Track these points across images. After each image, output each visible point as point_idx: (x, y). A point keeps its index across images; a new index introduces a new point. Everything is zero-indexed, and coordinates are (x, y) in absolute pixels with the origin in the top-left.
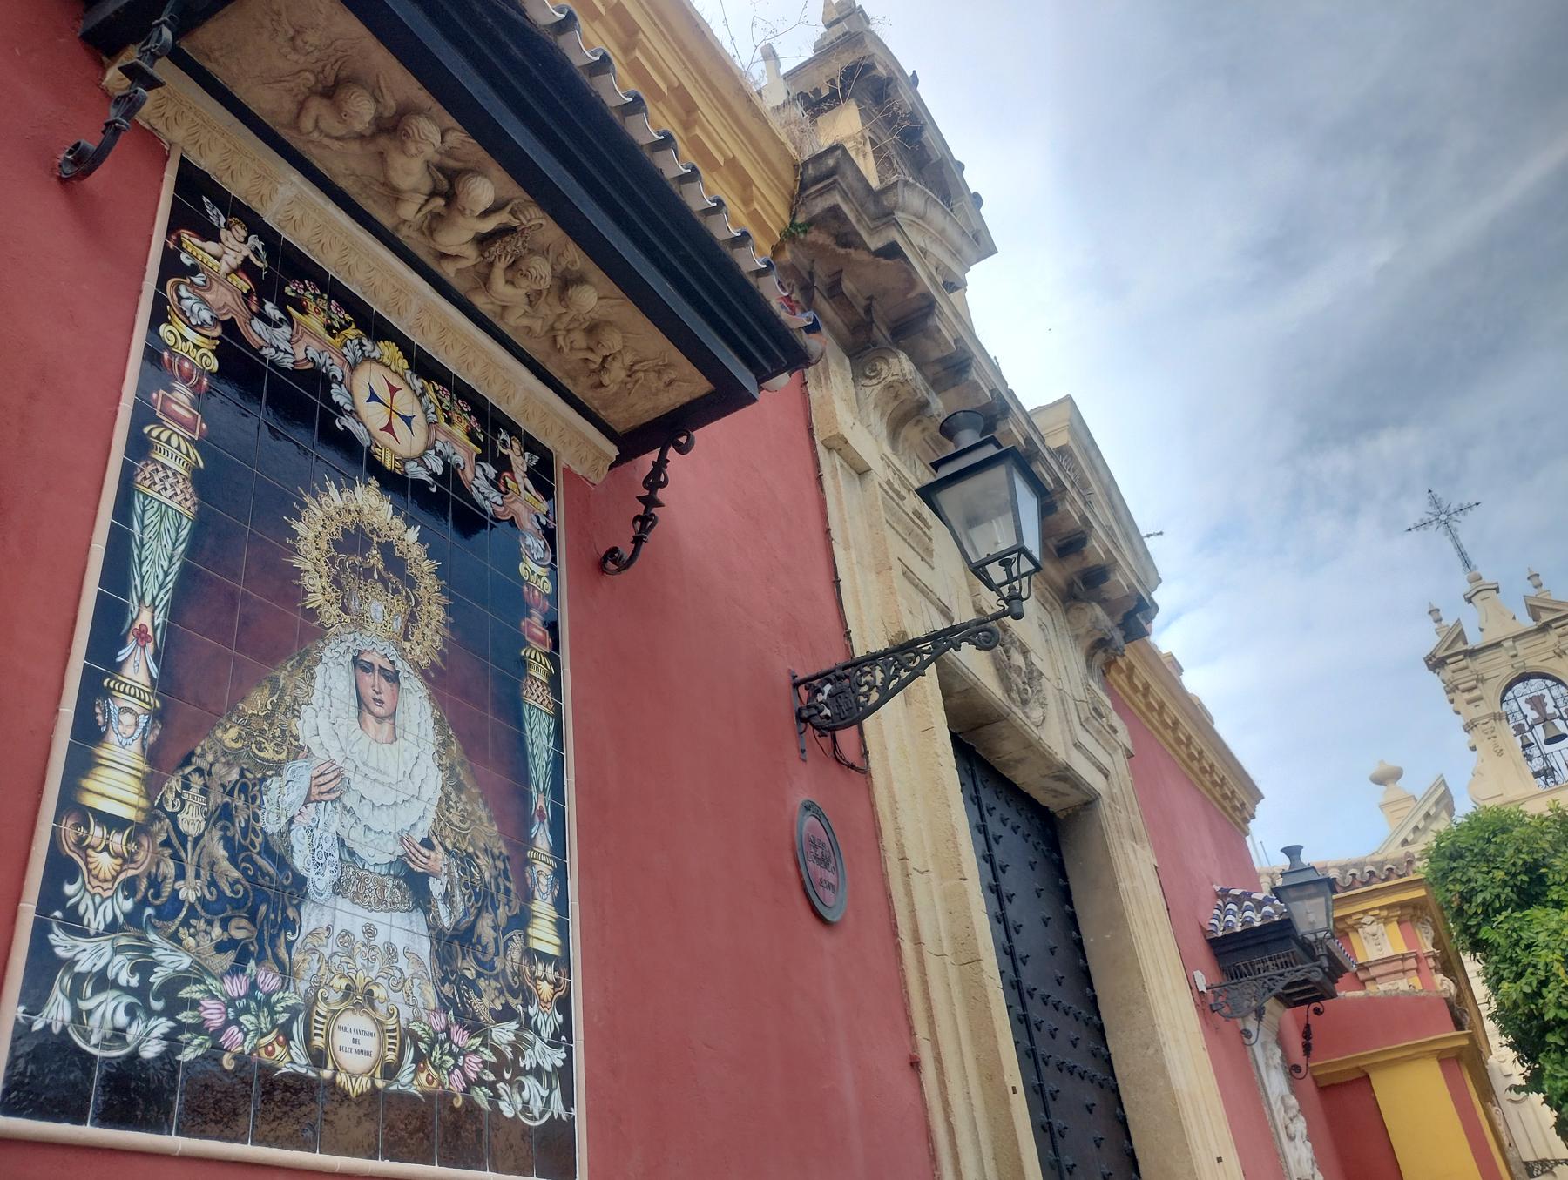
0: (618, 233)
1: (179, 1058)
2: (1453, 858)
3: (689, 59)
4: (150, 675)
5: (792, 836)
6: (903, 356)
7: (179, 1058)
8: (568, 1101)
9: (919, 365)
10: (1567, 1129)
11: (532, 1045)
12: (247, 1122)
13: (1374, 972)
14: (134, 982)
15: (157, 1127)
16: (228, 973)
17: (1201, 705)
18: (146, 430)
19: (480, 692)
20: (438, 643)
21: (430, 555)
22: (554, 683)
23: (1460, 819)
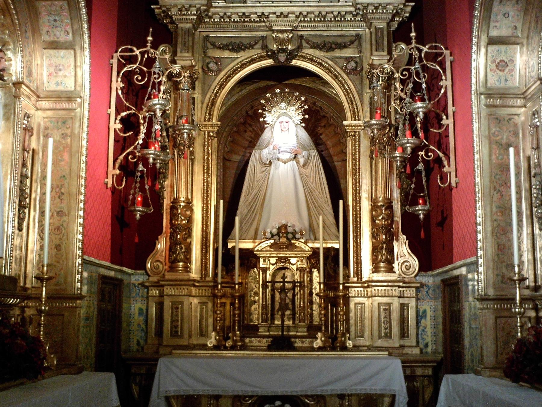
0: (449, 102)
1: (532, 341)
2: (185, 44)
3: (446, 146)
4: (120, 196)
5: (526, 81)
6: (144, 372)
7: (532, 341)
8: (38, 145)
9: (529, 328)
10: (79, 2)
11: (295, 342)
12: (53, 236)
13: (361, 348)
14: (258, 20)
15: (239, 270)
16: (431, 211)
17: (500, 37)
18: (19, 338)
19: (77, 351)
20: (283, 105)
21: (145, 134)
22: (8, 217)
23: (473, 46)
